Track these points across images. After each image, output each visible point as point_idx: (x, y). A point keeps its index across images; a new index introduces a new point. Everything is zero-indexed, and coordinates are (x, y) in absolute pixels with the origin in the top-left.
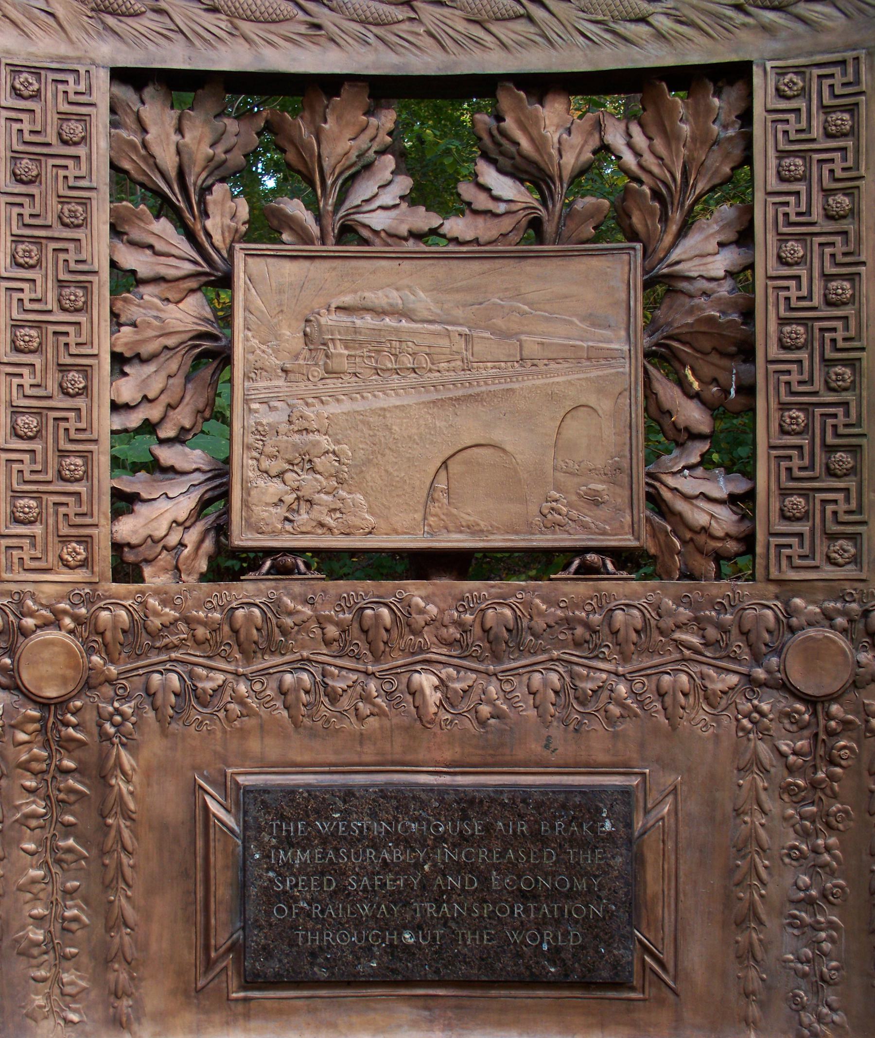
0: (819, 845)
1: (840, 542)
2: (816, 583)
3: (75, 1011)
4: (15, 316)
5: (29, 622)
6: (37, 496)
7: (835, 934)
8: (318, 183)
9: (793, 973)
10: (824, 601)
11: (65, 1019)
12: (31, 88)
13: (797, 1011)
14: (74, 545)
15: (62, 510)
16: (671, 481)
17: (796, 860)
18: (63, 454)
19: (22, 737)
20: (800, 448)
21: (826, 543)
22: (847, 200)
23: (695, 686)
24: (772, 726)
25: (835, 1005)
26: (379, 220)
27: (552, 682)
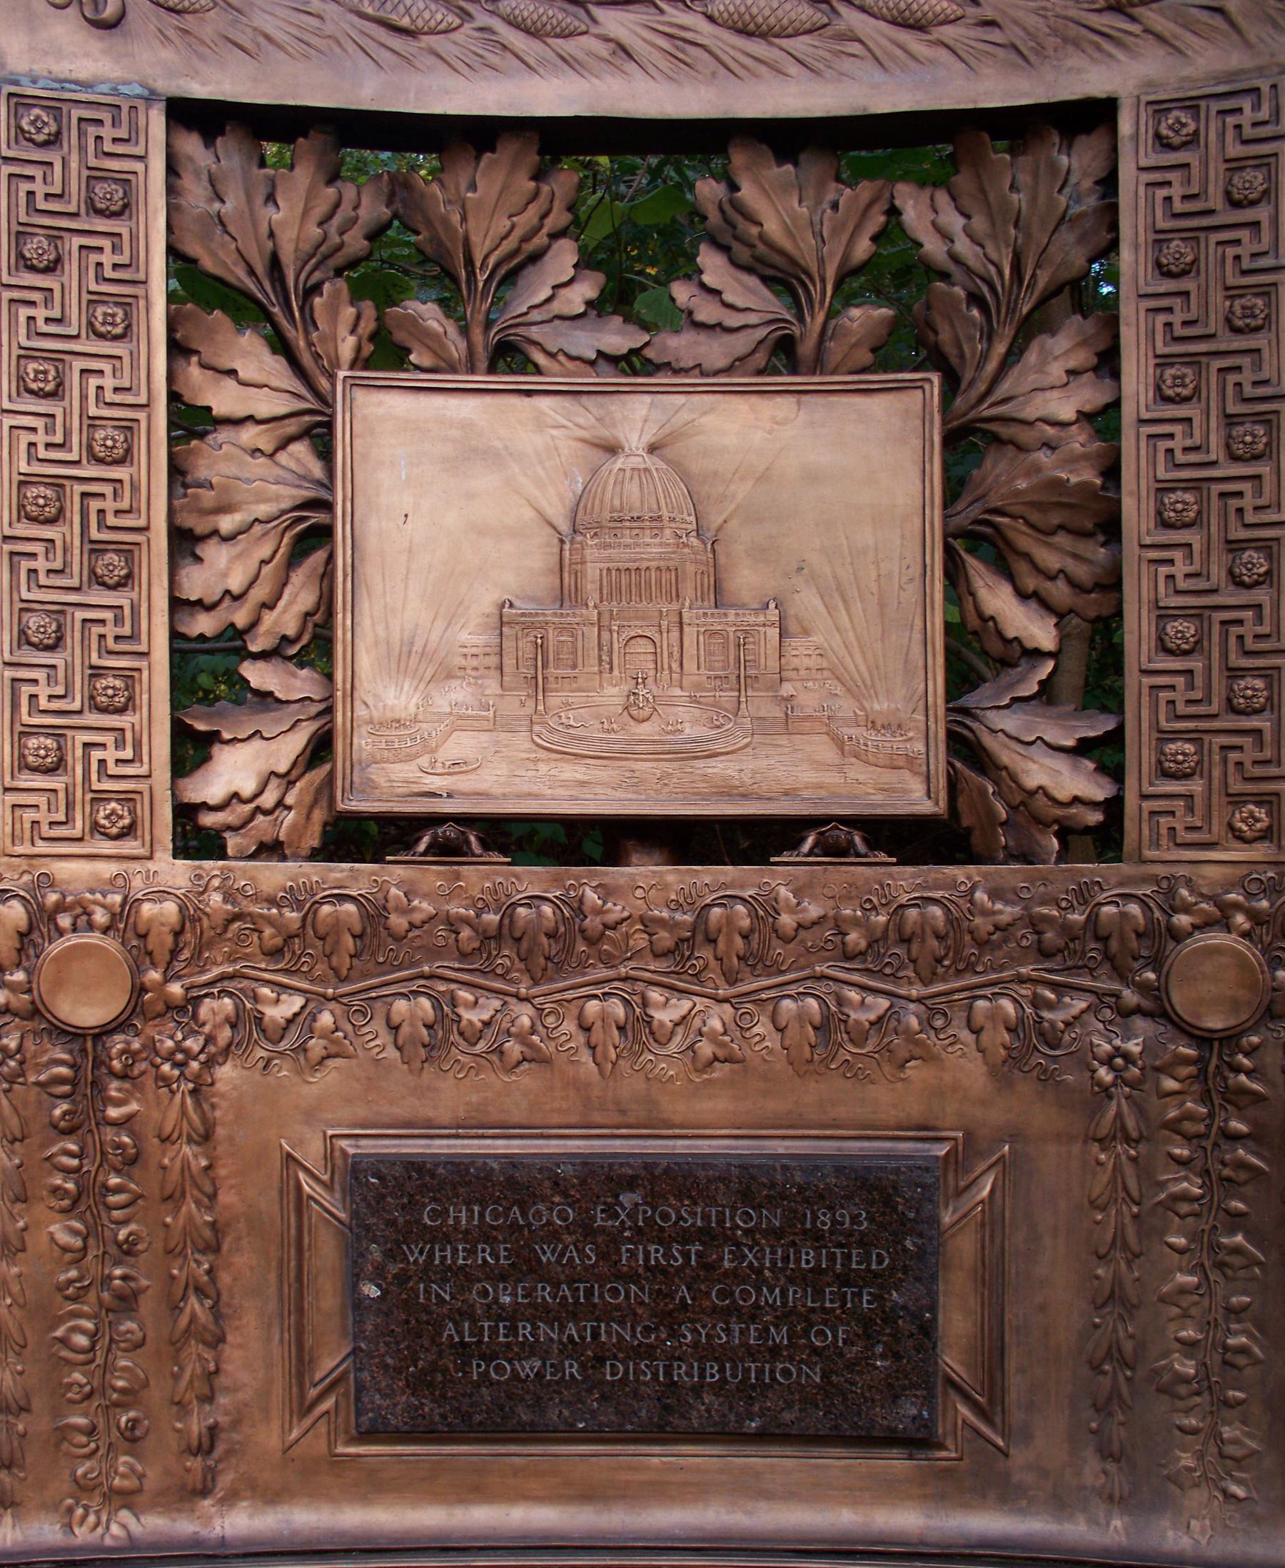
3: (1240, 1482)
4: (1162, 474)
5: (1183, 920)
6: (1196, 737)
11: (1224, 1492)
12: (1184, 131)
14: (1251, 807)
15: (1234, 756)
18: (1234, 673)
19: (1170, 1084)
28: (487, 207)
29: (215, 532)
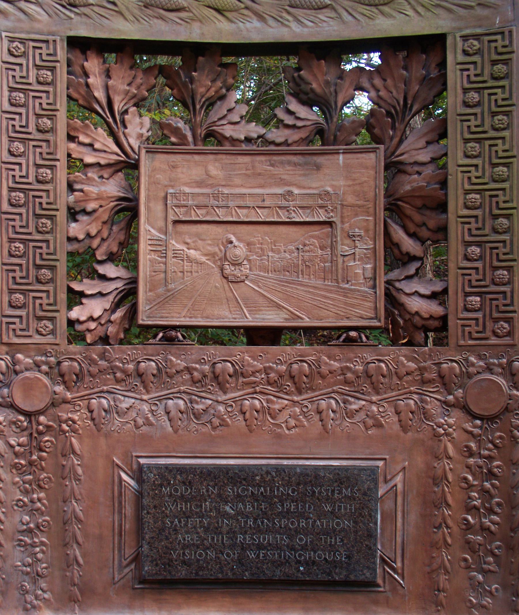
0: (34, 498)
1: (44, 322)
2: (30, 345)
7: (44, 548)
9: (20, 573)
10: (35, 356)
13: (24, 595)
17: (21, 507)
20: (20, 265)
21: (36, 322)
22: (49, 122)
23: (188, 407)
24: (5, 429)
25: (45, 589)
26: (228, 131)
27: (103, 405)
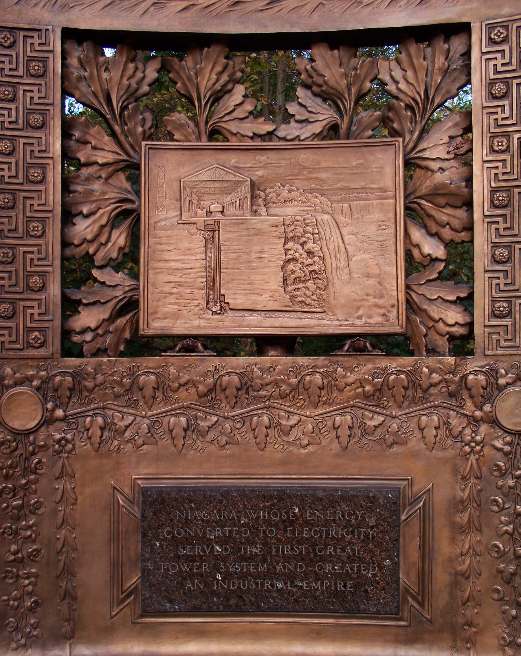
8: (196, 104)
16: (422, 290)
28: (205, 72)
29: (81, 213)
